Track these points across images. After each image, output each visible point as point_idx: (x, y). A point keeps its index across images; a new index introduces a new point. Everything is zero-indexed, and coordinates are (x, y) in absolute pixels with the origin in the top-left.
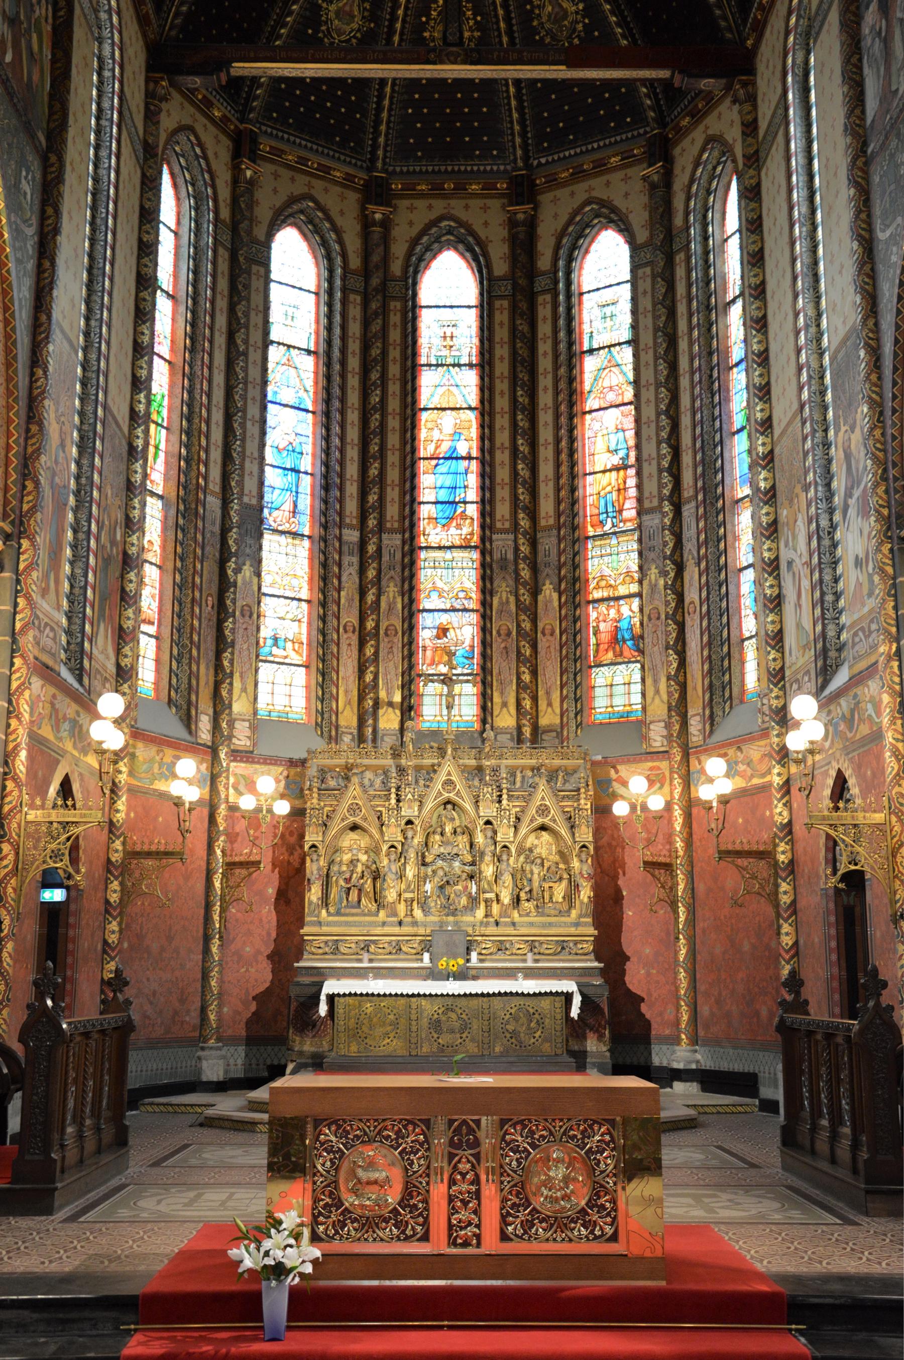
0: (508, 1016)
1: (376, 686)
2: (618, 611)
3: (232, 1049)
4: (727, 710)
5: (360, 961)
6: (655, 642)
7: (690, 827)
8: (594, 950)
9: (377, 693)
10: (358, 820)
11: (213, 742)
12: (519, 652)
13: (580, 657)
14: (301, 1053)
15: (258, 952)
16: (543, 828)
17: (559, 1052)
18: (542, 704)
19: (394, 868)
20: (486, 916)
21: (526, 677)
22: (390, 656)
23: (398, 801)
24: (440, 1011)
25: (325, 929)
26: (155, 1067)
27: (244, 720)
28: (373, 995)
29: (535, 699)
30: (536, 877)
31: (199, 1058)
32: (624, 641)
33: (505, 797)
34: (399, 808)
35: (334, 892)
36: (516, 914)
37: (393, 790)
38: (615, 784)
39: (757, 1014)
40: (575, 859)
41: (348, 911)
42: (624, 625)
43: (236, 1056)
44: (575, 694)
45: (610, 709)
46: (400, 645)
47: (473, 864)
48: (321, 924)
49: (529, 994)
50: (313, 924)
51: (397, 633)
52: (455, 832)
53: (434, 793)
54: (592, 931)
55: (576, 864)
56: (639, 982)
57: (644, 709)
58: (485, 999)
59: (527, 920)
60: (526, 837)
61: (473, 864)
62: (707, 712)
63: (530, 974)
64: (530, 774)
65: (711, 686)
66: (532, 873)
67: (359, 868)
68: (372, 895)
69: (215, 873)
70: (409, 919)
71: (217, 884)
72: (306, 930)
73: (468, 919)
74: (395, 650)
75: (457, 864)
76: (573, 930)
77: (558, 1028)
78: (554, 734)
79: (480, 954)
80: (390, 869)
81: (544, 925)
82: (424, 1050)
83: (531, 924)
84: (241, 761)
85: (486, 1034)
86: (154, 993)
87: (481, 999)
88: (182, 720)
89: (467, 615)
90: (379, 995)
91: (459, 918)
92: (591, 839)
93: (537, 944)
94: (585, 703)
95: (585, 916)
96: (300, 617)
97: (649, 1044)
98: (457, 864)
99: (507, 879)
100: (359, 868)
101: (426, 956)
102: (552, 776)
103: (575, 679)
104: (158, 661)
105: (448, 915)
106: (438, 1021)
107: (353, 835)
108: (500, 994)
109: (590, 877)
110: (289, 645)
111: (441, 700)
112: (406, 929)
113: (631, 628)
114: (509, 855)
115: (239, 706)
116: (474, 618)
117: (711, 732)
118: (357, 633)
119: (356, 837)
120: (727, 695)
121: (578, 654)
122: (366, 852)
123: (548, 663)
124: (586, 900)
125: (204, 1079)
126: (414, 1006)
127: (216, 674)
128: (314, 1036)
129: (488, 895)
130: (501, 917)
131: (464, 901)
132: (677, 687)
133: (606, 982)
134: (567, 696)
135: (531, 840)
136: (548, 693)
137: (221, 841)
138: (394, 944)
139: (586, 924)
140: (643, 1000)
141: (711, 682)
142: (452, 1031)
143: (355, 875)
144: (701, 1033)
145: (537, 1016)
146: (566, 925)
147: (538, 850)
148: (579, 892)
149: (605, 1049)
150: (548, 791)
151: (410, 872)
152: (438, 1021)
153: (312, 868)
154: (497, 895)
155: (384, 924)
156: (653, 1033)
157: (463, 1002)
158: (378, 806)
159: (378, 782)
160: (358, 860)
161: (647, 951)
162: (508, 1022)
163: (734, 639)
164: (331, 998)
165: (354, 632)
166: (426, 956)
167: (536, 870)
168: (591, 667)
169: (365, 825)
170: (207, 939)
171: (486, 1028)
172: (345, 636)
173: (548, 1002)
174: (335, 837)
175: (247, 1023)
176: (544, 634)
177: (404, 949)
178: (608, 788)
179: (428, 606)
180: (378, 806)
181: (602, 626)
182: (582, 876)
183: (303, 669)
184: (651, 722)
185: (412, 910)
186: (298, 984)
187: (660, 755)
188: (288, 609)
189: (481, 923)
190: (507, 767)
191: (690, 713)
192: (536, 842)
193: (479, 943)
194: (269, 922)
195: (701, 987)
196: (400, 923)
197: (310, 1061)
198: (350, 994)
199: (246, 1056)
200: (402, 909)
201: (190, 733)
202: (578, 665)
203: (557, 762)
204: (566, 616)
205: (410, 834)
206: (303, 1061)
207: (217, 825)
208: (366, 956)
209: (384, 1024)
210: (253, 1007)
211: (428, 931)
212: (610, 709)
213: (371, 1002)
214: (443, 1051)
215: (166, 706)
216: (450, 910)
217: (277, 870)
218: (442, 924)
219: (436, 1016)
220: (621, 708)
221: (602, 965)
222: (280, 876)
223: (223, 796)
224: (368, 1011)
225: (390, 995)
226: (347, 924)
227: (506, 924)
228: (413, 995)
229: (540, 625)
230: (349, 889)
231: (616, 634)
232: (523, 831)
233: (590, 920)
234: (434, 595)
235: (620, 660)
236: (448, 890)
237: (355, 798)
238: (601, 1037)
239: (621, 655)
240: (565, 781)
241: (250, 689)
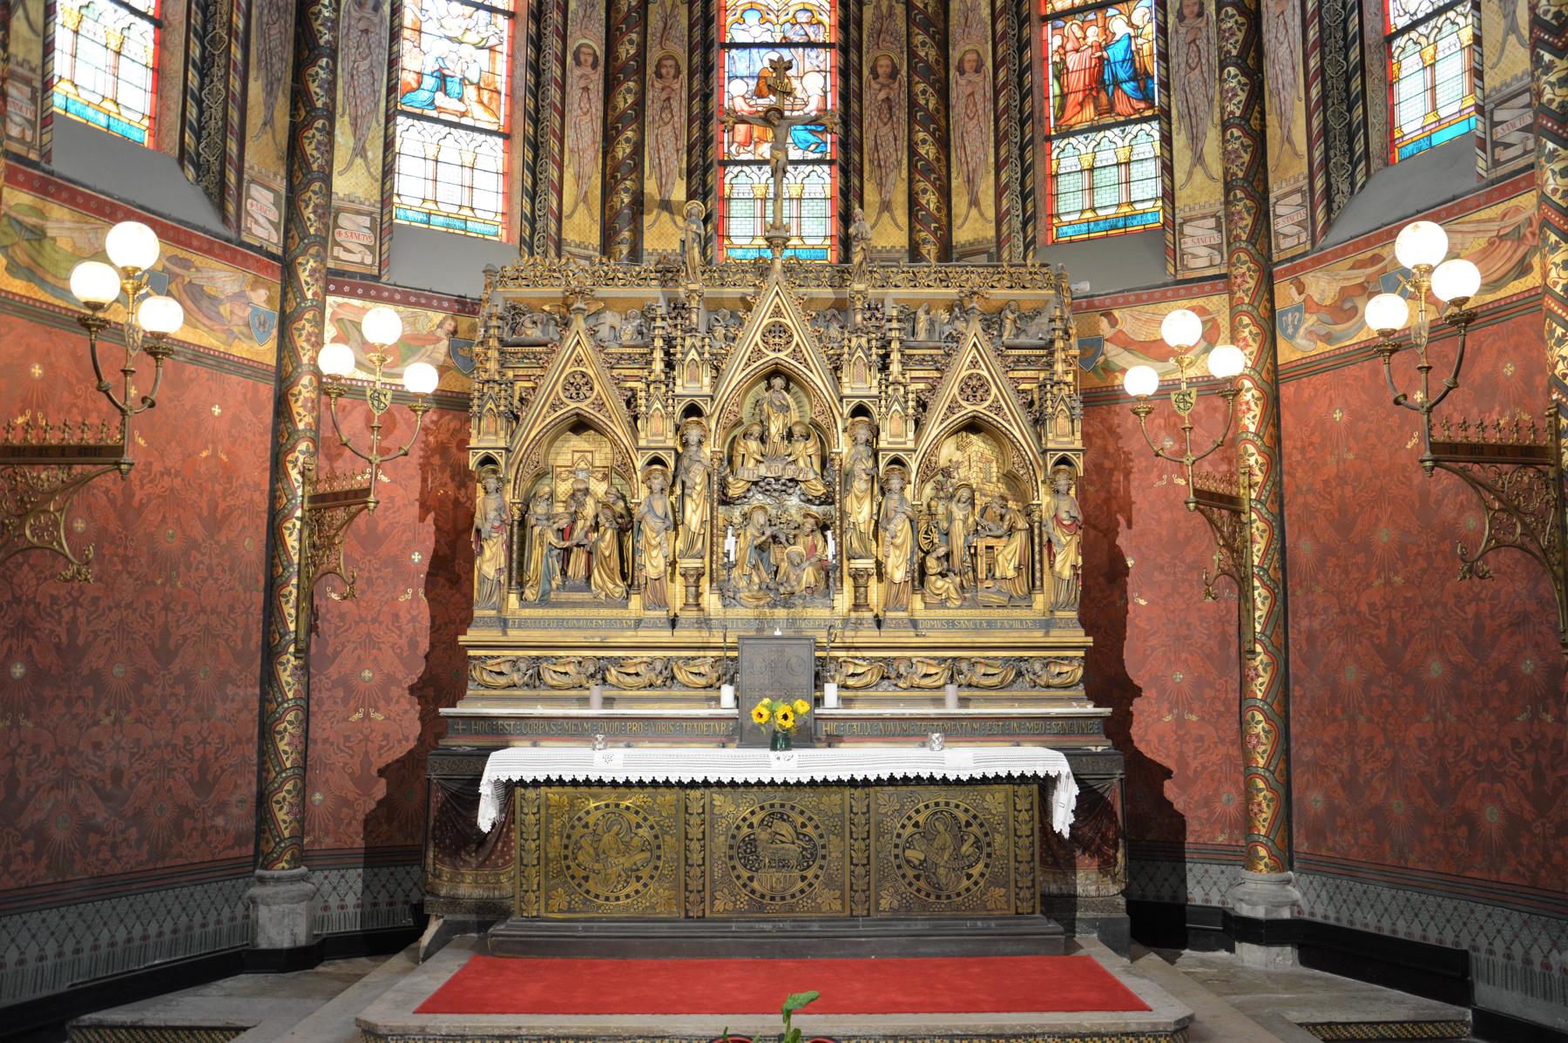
0: (910, 830)
1: (638, 167)
2: (1105, 29)
3: (334, 876)
4: (1360, 178)
5: (585, 701)
6: (1193, 61)
7: (1277, 426)
8: (1084, 679)
9: (640, 180)
10: (585, 407)
11: (285, 249)
12: (912, 104)
13: (1031, 115)
14: (453, 902)
15: (391, 680)
16: (973, 426)
17: (1025, 907)
18: (960, 203)
19: (661, 505)
20: (856, 607)
21: (928, 151)
22: (666, 116)
23: (670, 365)
24: (755, 820)
25: (514, 635)
26: (121, 935)
27: (358, 213)
28: (600, 783)
29: (945, 194)
30: (958, 529)
31: (253, 900)
32: (1117, 83)
33: (895, 356)
34: (669, 381)
35: (537, 558)
36: (917, 603)
37: (659, 343)
38: (1109, 348)
39: (1470, 821)
40: (1042, 489)
41: (564, 596)
42: (1117, 53)
43: (342, 889)
44: (1023, 184)
45: (1089, 215)
46: (685, 95)
47: (827, 500)
48: (505, 623)
49: (958, 781)
50: (487, 623)
51: (678, 72)
52: (789, 436)
53: (743, 350)
54: (1079, 637)
55: (1044, 499)
56: (1161, 738)
57: (1169, 196)
58: (858, 792)
59: (941, 617)
60: (937, 445)
61: (827, 500)
62: (1319, 184)
63: (958, 730)
64: (945, 317)
65: (1325, 130)
66: (950, 518)
67: (590, 509)
68: (615, 562)
69: (287, 518)
70: (692, 614)
71: (292, 541)
72: (472, 635)
73: (819, 612)
74: (675, 104)
75: (793, 501)
76: (1038, 636)
77: (1024, 855)
78: (983, 259)
79: (845, 687)
80: (651, 508)
81: (977, 627)
82: (719, 905)
83: (951, 624)
84: (352, 294)
85: (860, 870)
86: (117, 775)
87: (847, 792)
88: (209, 195)
89: (813, 53)
90: (614, 784)
91: (798, 612)
92: (1078, 444)
93: (964, 666)
94: (1040, 204)
95: (1066, 606)
96: (493, 41)
97: (1182, 860)
98: (793, 501)
99: (900, 527)
100: (590, 509)
101: (727, 693)
102: (992, 321)
103: (1022, 157)
104: (158, 71)
105: (775, 606)
106: (751, 842)
107: (578, 442)
108: (892, 780)
109: (1075, 525)
110: (471, 92)
111: (764, 208)
112: (684, 635)
113: (1131, 58)
114: (905, 481)
115: (351, 182)
116: (825, 59)
117: (1329, 224)
118: (601, 69)
119: (585, 446)
120: (1359, 148)
121: (1027, 110)
122: (605, 477)
123: (971, 125)
124: (1067, 573)
125: (263, 944)
126: (695, 808)
127: (294, 109)
128: (481, 865)
129: (859, 564)
130: (886, 608)
131: (808, 575)
132: (1247, 141)
133: (1116, 746)
134: (1007, 186)
135: (948, 452)
136: (970, 181)
137: (301, 451)
138: (659, 666)
139: (1066, 624)
140: (1168, 773)
141: (1325, 121)
142: (783, 864)
143: (580, 523)
144: (1302, 845)
145: (974, 829)
146: (1023, 625)
147: (963, 472)
148: (1052, 555)
149: (1114, 889)
150: (987, 348)
151: (694, 515)
152: (751, 842)
153: (489, 506)
154: (879, 564)
155: (638, 623)
156: (1190, 839)
157: (808, 799)
158: (626, 378)
159: (628, 331)
160: (587, 491)
161: (1179, 677)
162: (909, 844)
163: (1371, 37)
164: (509, 789)
165: (594, 65)
166: (727, 693)
167: (959, 514)
168: (1049, 139)
169: (599, 417)
170: (271, 653)
171: (859, 857)
172: (578, 72)
173: (1000, 797)
174: (537, 442)
175: (366, 822)
176: (962, 72)
177: (679, 676)
178: (1095, 356)
179: (740, 37)
180: (626, 378)
181: (1072, 60)
182: (1059, 523)
183: (500, 141)
184: (1185, 222)
185: (698, 595)
186: (448, 753)
187: (1207, 286)
188: (471, 23)
189: (846, 621)
190: (896, 301)
191: (1275, 191)
192: (958, 456)
193: (841, 665)
194: (414, 619)
195: (1304, 752)
196: (673, 623)
197: (472, 918)
198: (548, 782)
199: (366, 887)
200: (677, 592)
201: (225, 219)
202: (1028, 129)
203: (1000, 294)
204: (1005, 34)
205: (693, 434)
206: (459, 917)
207: (291, 419)
208: (596, 692)
209: (627, 849)
210: (380, 790)
211: (731, 639)
212: (1089, 215)
213: (596, 797)
214: (761, 908)
215: (177, 168)
216: (779, 594)
217: (431, 517)
218: (762, 623)
219: (746, 830)
220: (1112, 211)
221: (1106, 711)
222: (438, 529)
223: (305, 360)
224: (591, 820)
225: (641, 784)
226: (561, 623)
227: (898, 624)
228: (693, 784)
229: (955, 56)
230: (567, 551)
231: (1101, 72)
232: (933, 429)
233: (1074, 615)
234: (752, 18)
235: (1109, 120)
236: (776, 553)
237: (579, 362)
238: (1106, 866)
239: (1111, 108)
240: (1019, 331)
241: (375, 153)
